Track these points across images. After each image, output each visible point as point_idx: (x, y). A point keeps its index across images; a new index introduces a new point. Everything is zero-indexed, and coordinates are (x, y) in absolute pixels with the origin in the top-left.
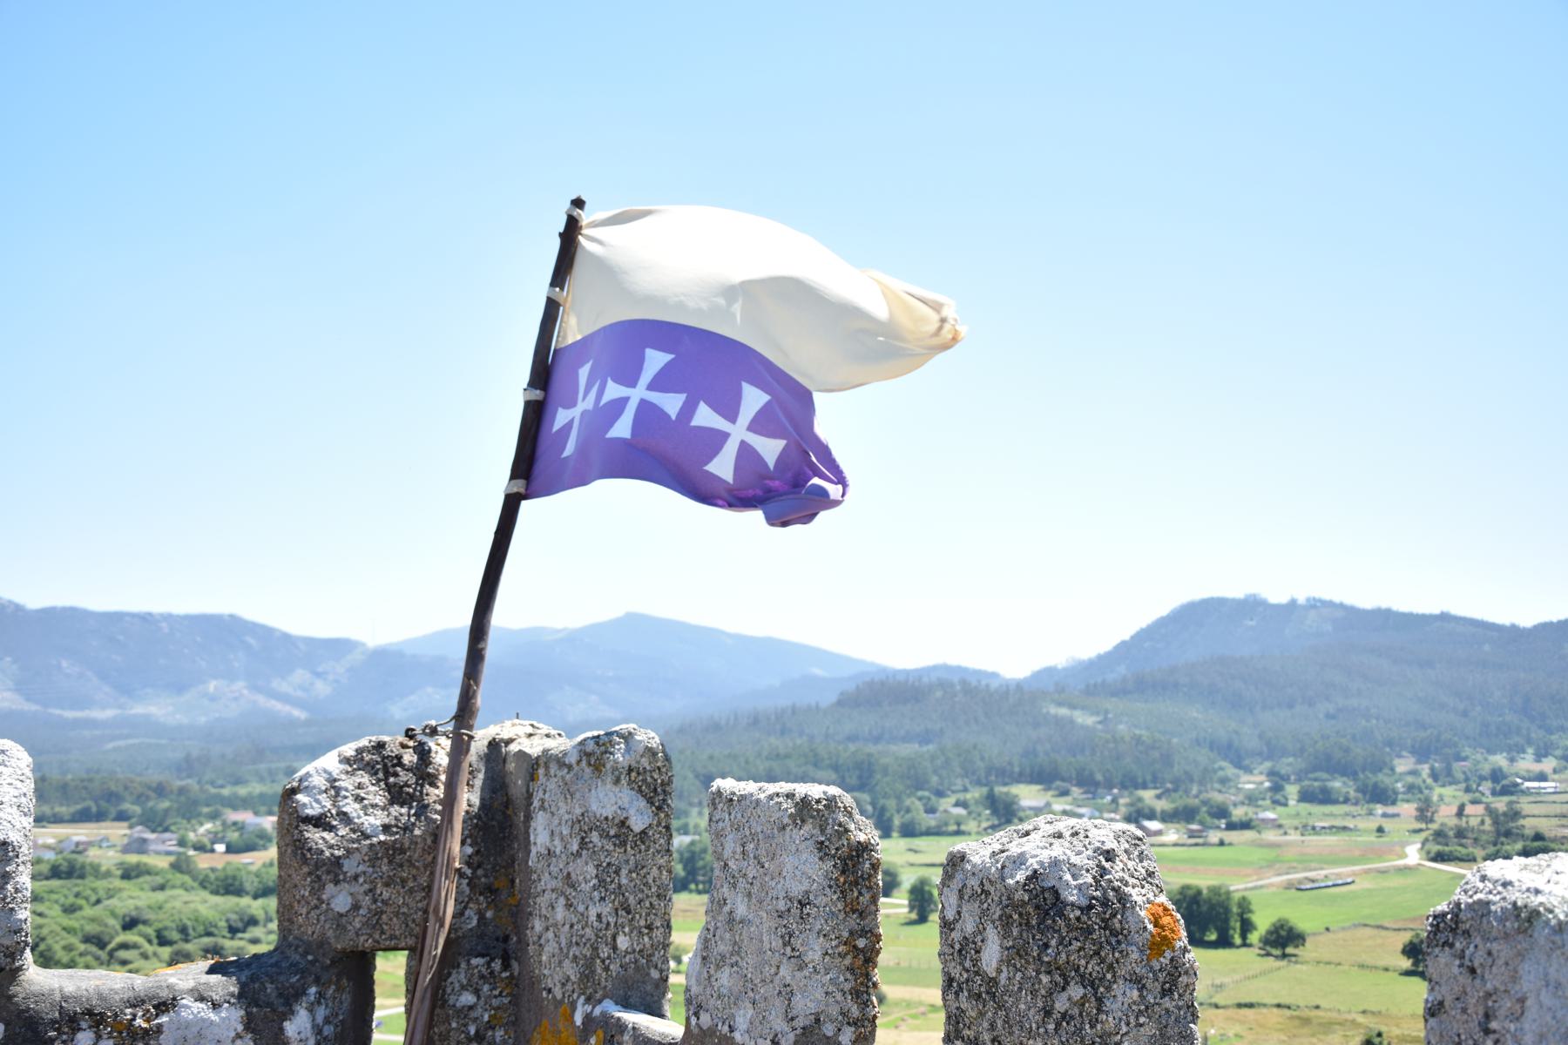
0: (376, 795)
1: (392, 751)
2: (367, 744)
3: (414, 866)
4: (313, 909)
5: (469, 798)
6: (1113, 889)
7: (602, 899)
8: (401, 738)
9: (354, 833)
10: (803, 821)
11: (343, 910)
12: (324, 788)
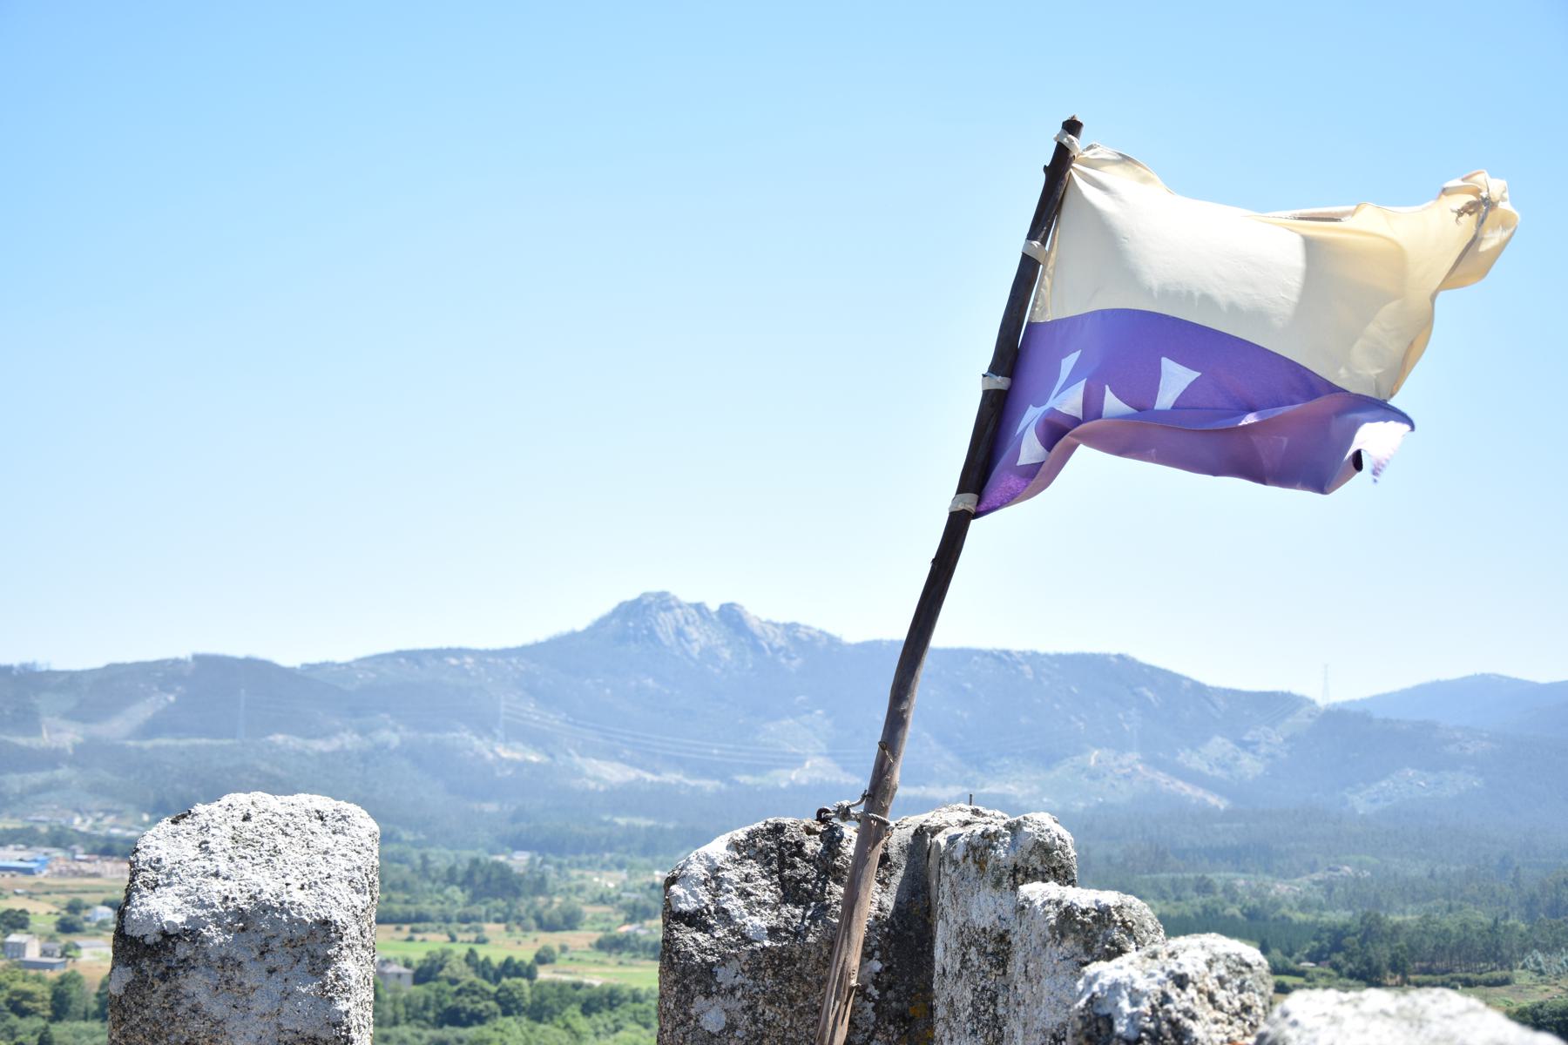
0: (766, 890)
1: (792, 837)
2: (762, 827)
3: (805, 981)
4: (678, 1025)
5: (877, 899)
6: (1170, 1021)
7: (974, 1032)
8: (810, 821)
9: (733, 935)
10: (1063, 935)
11: (715, 1030)
12: (702, 878)
